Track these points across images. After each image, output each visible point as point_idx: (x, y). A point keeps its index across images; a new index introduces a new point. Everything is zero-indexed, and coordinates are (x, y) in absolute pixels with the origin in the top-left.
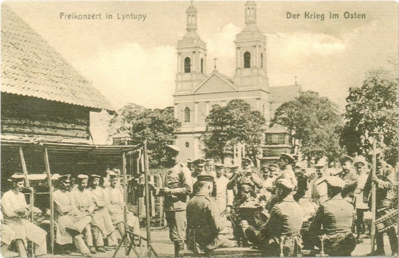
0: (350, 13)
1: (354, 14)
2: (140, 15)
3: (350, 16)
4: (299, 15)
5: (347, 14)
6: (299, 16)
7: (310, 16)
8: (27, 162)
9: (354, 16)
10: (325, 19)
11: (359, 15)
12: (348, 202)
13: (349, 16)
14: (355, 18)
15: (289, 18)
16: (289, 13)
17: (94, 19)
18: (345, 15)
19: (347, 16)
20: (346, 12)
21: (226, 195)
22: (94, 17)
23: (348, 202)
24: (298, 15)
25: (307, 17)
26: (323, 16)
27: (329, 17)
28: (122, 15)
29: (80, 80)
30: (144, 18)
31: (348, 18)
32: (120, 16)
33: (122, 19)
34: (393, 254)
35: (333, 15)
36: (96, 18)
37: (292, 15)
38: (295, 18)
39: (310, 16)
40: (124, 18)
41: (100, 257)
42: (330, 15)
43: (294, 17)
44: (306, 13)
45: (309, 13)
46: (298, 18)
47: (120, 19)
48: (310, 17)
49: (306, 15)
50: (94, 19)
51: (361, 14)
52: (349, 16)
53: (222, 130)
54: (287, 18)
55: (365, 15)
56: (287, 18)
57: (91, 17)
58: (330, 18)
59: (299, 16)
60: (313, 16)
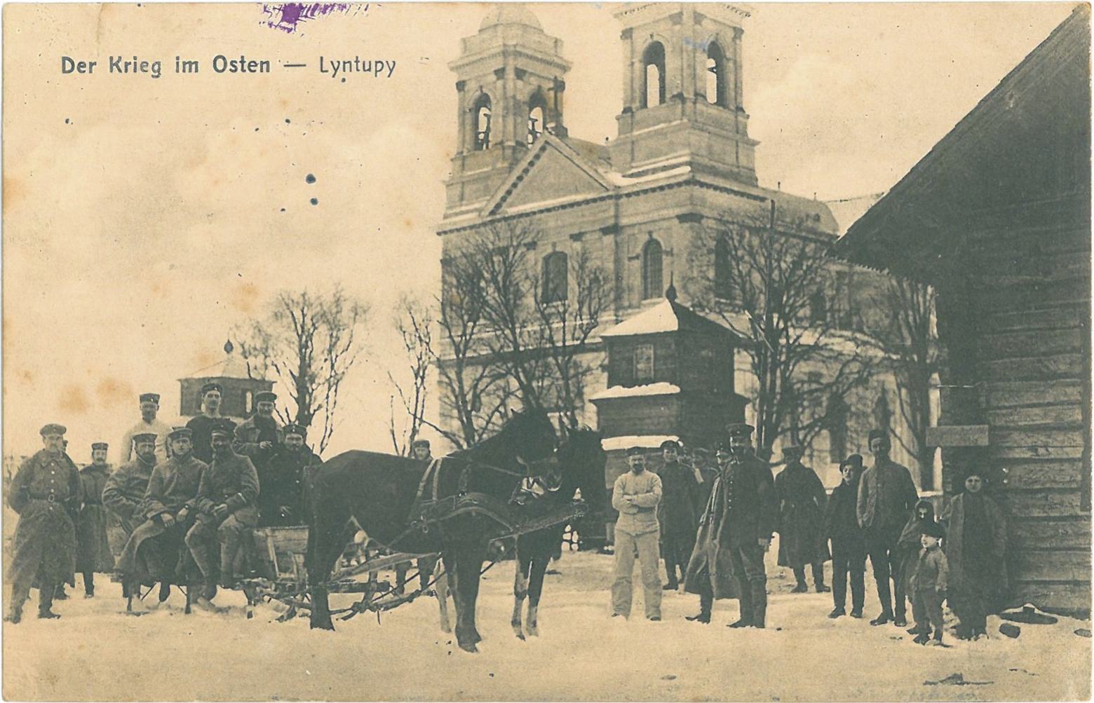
3: (229, 67)
4: (95, 64)
5: (220, 62)
6: (94, 67)
8: (744, 609)
9: (239, 65)
14: (358, 70)
15: (70, 71)
16: (70, 60)
18: (215, 61)
19: (220, 67)
24: (92, 64)
25: (115, 67)
26: (156, 67)
28: (332, 63)
30: (391, 71)
31: (223, 70)
32: (327, 66)
33: (332, 71)
35: (184, 64)
36: (91, 72)
38: (255, 71)
40: (336, 70)
41: (866, 584)
42: (178, 63)
43: (82, 69)
44: (111, 58)
46: (91, 72)
47: (327, 71)
49: (112, 65)
53: (569, 379)
54: (64, 71)
55: (267, 63)
56: (64, 71)
58: (177, 71)
60: (131, 68)
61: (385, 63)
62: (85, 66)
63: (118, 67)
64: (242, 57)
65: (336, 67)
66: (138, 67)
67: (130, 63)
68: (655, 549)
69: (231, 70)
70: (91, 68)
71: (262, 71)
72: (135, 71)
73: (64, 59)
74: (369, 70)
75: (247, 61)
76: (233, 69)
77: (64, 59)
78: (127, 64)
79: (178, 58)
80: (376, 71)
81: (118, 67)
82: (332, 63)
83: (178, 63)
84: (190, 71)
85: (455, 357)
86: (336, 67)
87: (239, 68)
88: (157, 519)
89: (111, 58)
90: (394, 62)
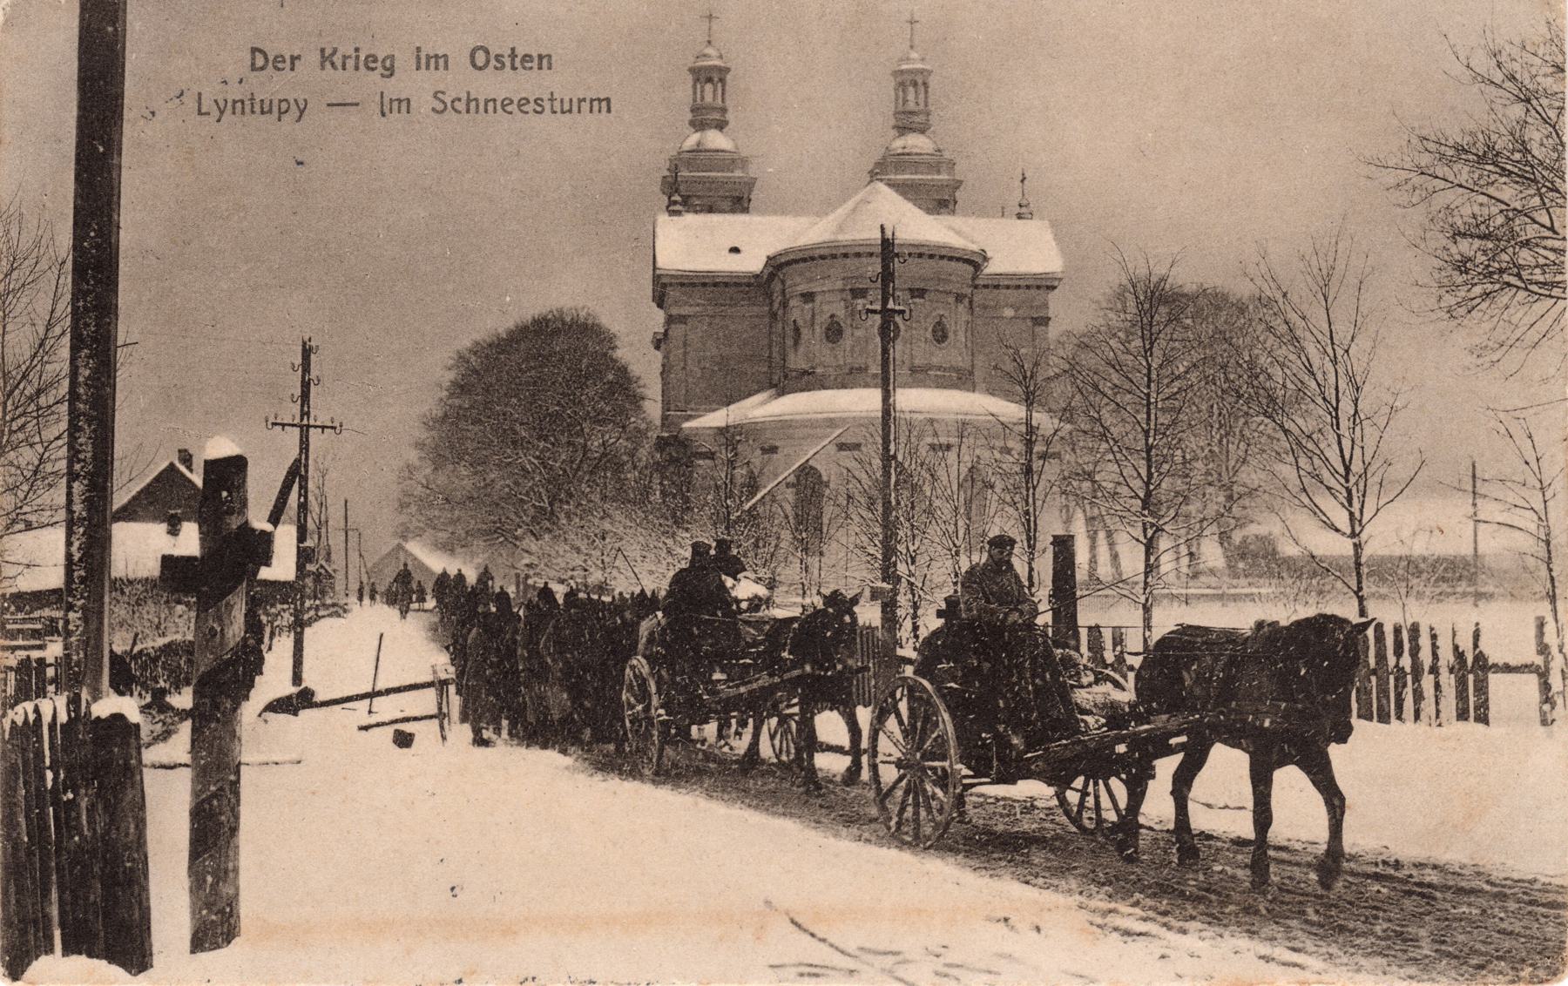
0: (494, 51)
1: (546, 97)
2: (286, 100)
3: (493, 62)
5: (480, 58)
7: (339, 63)
9: (547, 105)
10: (396, 74)
11: (527, 58)
12: (1454, 635)
13: (488, 61)
14: (253, 112)
15: (262, 68)
16: (261, 51)
17: (511, 113)
20: (480, 69)
21: (1222, 805)
22: (524, 108)
23: (1454, 635)
24: (294, 59)
26: (388, 64)
27: (414, 67)
29: (1002, 924)
30: (302, 112)
33: (217, 114)
34: (546, 583)
35: (428, 57)
36: (292, 69)
37: (271, 58)
39: (339, 63)
40: (222, 112)
42: (418, 58)
43: (280, 65)
44: (323, 50)
45: (335, 51)
46: (292, 69)
47: (208, 114)
48: (340, 67)
50: (511, 113)
51: (535, 55)
52: (488, 61)
57: (513, 108)
59: (297, 62)
60: (350, 63)
61: (292, 102)
62: (375, 61)
63: (333, 64)
64: (513, 50)
65: (302, 107)
66: (361, 64)
67: (350, 57)
68: (142, 474)
69: (496, 68)
70: (293, 63)
71: (468, 111)
72: (495, 112)
73: (254, 50)
74: (270, 111)
75: (520, 52)
76: (539, 109)
77: (254, 50)
78: (345, 58)
79: (419, 49)
80: (280, 113)
81: (333, 64)
82: (216, 101)
83: (418, 58)
84: (437, 68)
85: (1034, 414)
86: (302, 107)
87: (508, 64)
88: (632, 707)
89: (323, 50)
90: (305, 100)
